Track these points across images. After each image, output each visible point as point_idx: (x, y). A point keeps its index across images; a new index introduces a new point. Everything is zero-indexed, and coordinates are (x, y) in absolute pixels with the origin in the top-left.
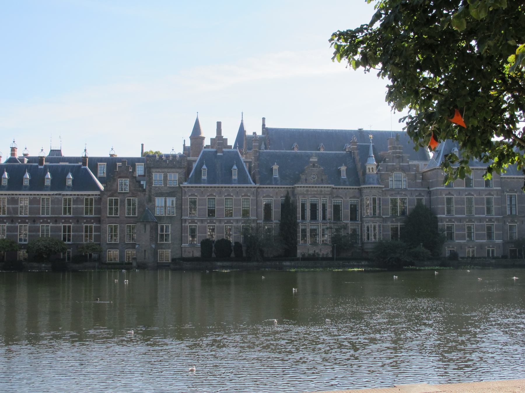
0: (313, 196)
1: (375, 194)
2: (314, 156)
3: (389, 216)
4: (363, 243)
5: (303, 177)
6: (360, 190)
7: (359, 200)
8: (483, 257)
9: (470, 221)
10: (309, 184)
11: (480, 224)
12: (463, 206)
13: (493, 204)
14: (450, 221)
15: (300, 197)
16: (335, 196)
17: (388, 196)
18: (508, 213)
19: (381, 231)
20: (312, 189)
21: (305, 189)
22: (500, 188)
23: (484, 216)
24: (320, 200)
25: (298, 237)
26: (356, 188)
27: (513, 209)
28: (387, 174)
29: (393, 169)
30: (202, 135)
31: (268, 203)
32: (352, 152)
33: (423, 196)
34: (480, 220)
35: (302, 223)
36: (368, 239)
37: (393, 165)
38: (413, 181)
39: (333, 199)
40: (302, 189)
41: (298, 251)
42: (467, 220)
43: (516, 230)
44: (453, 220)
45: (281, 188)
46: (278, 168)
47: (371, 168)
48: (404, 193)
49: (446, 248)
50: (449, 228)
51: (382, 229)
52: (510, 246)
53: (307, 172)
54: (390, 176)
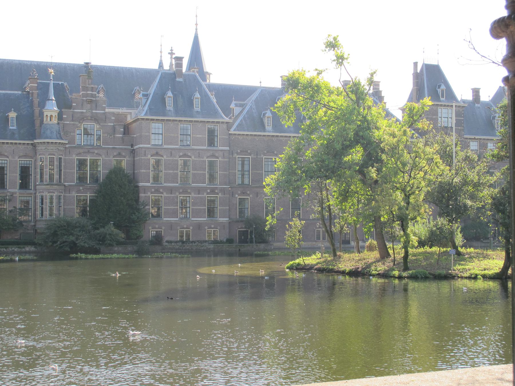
1: (52, 153)
3: (74, 184)
7: (33, 160)
8: (198, 241)
9: (185, 192)
11: (198, 195)
14: (157, 191)
17: (74, 156)
19: (62, 204)
23: (205, 185)
26: (28, 144)
27: (246, 176)
29: (82, 118)
31: (25, 166)
32: (30, 92)
33: (125, 157)
34: (199, 191)
36: (42, 215)
42: (181, 191)
43: (248, 205)
46: (17, 117)
47: (49, 116)
48: (96, 152)
49: (150, 228)
50: (156, 203)
51: (62, 201)
52: (240, 227)
54: (77, 127)
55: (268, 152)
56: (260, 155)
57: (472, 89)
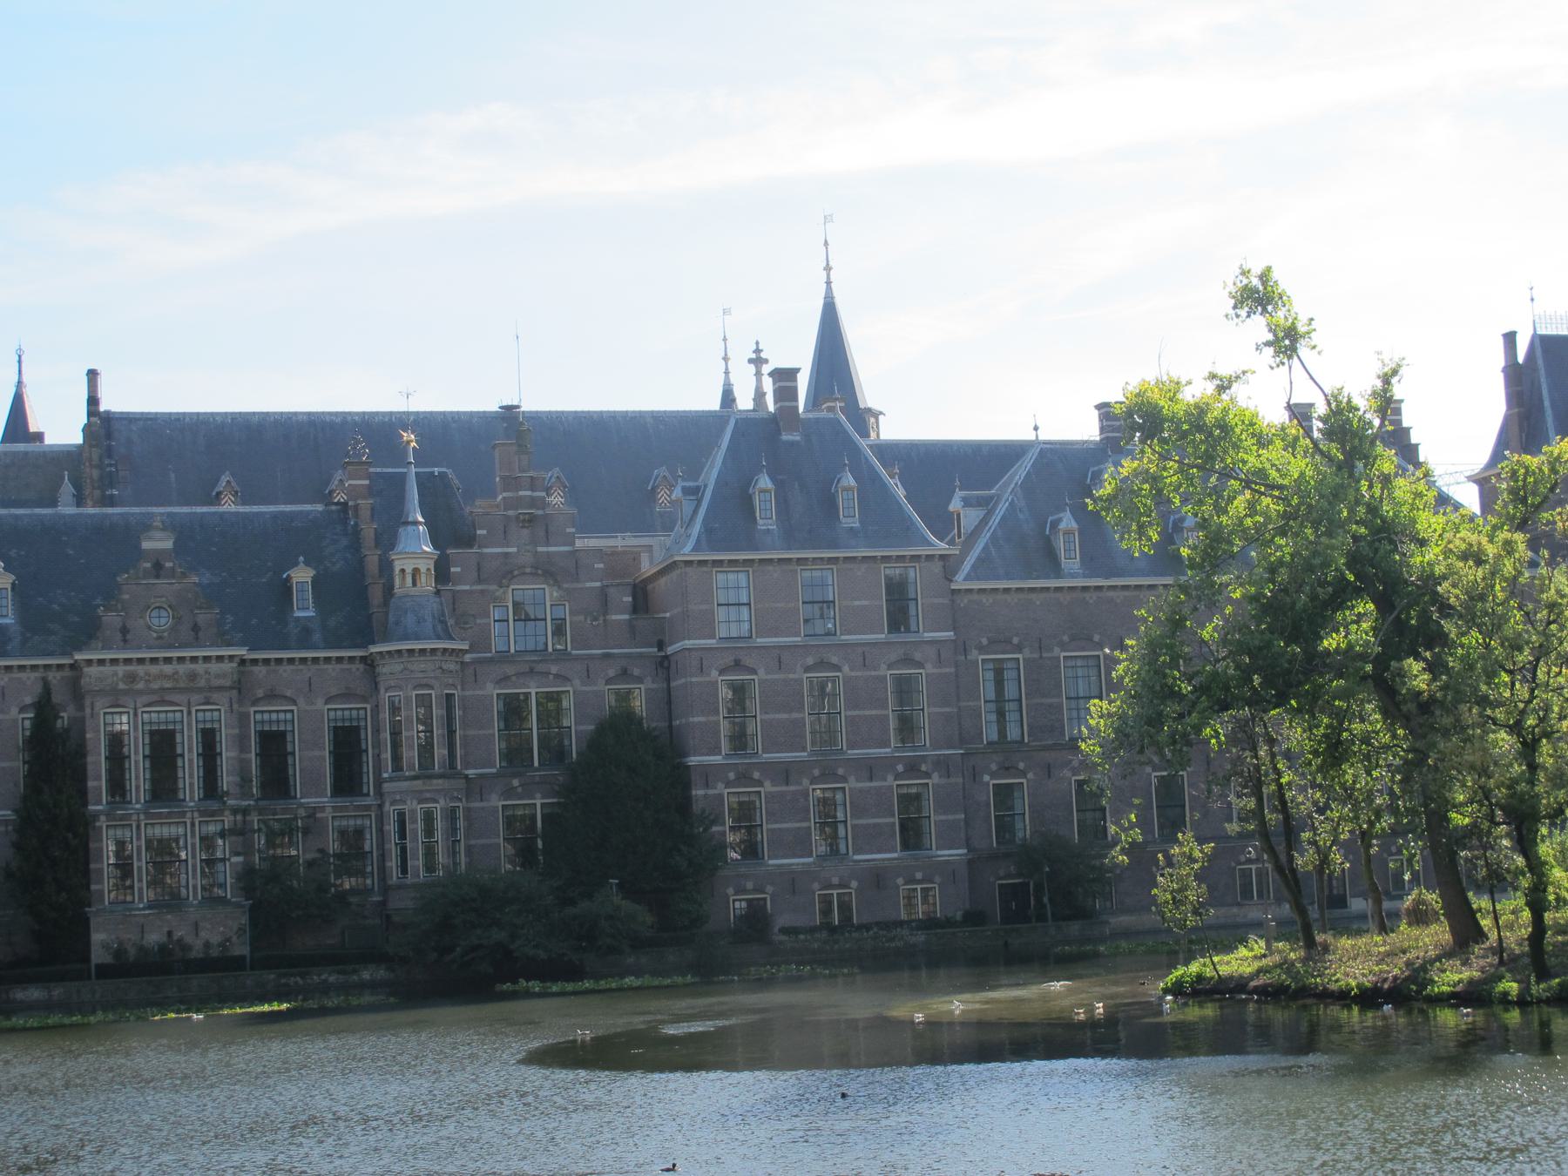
0: (155, 698)
1: (424, 681)
2: (157, 528)
3: (494, 770)
4: (386, 889)
5: (111, 619)
6: (369, 663)
7: (368, 706)
8: (877, 924)
10: (139, 648)
11: (868, 784)
12: (795, 715)
13: (924, 700)
14: (744, 777)
15: (98, 705)
16: (260, 693)
18: (990, 733)
19: (461, 835)
20: (154, 669)
21: (121, 670)
22: (952, 633)
24: (189, 713)
25: (93, 876)
27: (1012, 717)
28: (482, 591)
29: (508, 573)
30: (1413, 441)
32: (350, 503)
34: (871, 769)
35: (110, 816)
37: (506, 555)
38: (596, 619)
39: (252, 709)
40: (107, 669)
41: (97, 937)
42: (816, 772)
43: (1023, 804)
44: (756, 775)
45: (22, 668)
47: (409, 570)
48: (554, 669)
50: (745, 814)
51: (461, 824)
52: (1002, 873)
53: (126, 597)
54: (495, 599)
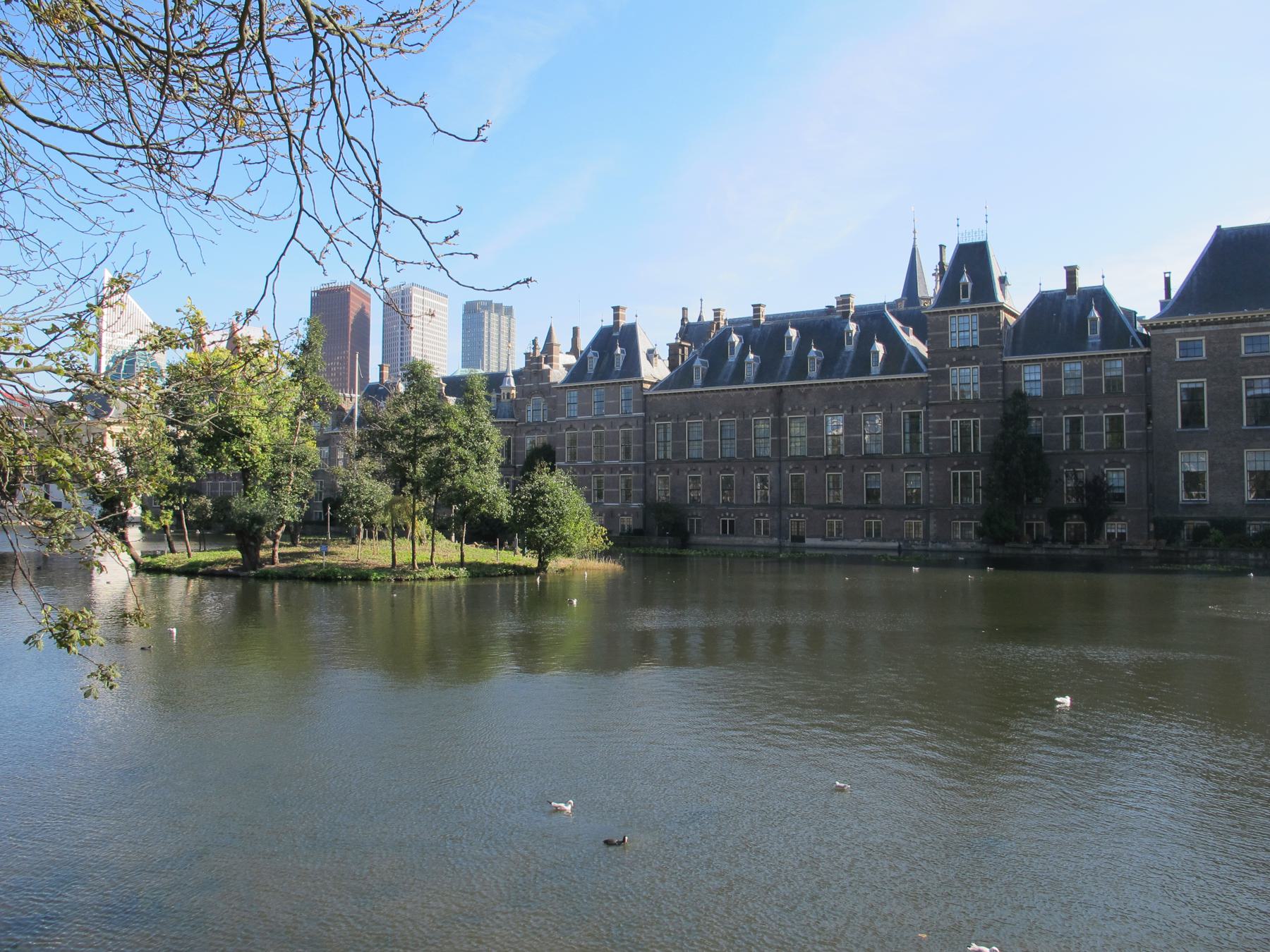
48: (542, 428)
55: (692, 414)
56: (748, 416)
57: (1065, 268)
